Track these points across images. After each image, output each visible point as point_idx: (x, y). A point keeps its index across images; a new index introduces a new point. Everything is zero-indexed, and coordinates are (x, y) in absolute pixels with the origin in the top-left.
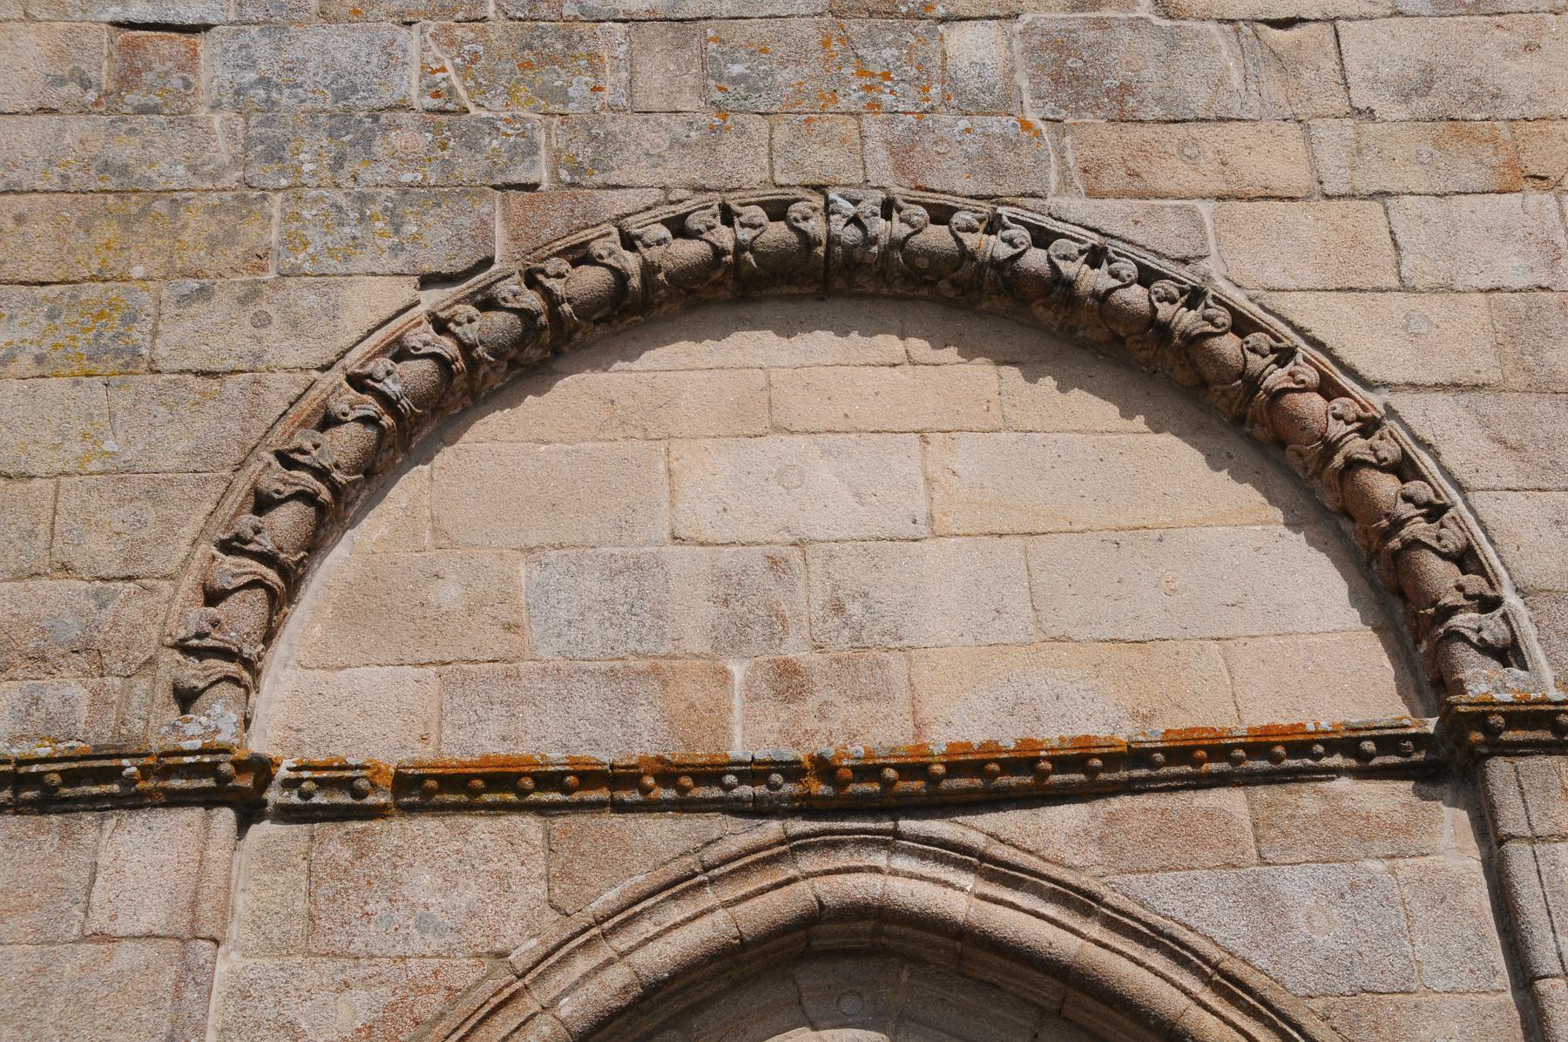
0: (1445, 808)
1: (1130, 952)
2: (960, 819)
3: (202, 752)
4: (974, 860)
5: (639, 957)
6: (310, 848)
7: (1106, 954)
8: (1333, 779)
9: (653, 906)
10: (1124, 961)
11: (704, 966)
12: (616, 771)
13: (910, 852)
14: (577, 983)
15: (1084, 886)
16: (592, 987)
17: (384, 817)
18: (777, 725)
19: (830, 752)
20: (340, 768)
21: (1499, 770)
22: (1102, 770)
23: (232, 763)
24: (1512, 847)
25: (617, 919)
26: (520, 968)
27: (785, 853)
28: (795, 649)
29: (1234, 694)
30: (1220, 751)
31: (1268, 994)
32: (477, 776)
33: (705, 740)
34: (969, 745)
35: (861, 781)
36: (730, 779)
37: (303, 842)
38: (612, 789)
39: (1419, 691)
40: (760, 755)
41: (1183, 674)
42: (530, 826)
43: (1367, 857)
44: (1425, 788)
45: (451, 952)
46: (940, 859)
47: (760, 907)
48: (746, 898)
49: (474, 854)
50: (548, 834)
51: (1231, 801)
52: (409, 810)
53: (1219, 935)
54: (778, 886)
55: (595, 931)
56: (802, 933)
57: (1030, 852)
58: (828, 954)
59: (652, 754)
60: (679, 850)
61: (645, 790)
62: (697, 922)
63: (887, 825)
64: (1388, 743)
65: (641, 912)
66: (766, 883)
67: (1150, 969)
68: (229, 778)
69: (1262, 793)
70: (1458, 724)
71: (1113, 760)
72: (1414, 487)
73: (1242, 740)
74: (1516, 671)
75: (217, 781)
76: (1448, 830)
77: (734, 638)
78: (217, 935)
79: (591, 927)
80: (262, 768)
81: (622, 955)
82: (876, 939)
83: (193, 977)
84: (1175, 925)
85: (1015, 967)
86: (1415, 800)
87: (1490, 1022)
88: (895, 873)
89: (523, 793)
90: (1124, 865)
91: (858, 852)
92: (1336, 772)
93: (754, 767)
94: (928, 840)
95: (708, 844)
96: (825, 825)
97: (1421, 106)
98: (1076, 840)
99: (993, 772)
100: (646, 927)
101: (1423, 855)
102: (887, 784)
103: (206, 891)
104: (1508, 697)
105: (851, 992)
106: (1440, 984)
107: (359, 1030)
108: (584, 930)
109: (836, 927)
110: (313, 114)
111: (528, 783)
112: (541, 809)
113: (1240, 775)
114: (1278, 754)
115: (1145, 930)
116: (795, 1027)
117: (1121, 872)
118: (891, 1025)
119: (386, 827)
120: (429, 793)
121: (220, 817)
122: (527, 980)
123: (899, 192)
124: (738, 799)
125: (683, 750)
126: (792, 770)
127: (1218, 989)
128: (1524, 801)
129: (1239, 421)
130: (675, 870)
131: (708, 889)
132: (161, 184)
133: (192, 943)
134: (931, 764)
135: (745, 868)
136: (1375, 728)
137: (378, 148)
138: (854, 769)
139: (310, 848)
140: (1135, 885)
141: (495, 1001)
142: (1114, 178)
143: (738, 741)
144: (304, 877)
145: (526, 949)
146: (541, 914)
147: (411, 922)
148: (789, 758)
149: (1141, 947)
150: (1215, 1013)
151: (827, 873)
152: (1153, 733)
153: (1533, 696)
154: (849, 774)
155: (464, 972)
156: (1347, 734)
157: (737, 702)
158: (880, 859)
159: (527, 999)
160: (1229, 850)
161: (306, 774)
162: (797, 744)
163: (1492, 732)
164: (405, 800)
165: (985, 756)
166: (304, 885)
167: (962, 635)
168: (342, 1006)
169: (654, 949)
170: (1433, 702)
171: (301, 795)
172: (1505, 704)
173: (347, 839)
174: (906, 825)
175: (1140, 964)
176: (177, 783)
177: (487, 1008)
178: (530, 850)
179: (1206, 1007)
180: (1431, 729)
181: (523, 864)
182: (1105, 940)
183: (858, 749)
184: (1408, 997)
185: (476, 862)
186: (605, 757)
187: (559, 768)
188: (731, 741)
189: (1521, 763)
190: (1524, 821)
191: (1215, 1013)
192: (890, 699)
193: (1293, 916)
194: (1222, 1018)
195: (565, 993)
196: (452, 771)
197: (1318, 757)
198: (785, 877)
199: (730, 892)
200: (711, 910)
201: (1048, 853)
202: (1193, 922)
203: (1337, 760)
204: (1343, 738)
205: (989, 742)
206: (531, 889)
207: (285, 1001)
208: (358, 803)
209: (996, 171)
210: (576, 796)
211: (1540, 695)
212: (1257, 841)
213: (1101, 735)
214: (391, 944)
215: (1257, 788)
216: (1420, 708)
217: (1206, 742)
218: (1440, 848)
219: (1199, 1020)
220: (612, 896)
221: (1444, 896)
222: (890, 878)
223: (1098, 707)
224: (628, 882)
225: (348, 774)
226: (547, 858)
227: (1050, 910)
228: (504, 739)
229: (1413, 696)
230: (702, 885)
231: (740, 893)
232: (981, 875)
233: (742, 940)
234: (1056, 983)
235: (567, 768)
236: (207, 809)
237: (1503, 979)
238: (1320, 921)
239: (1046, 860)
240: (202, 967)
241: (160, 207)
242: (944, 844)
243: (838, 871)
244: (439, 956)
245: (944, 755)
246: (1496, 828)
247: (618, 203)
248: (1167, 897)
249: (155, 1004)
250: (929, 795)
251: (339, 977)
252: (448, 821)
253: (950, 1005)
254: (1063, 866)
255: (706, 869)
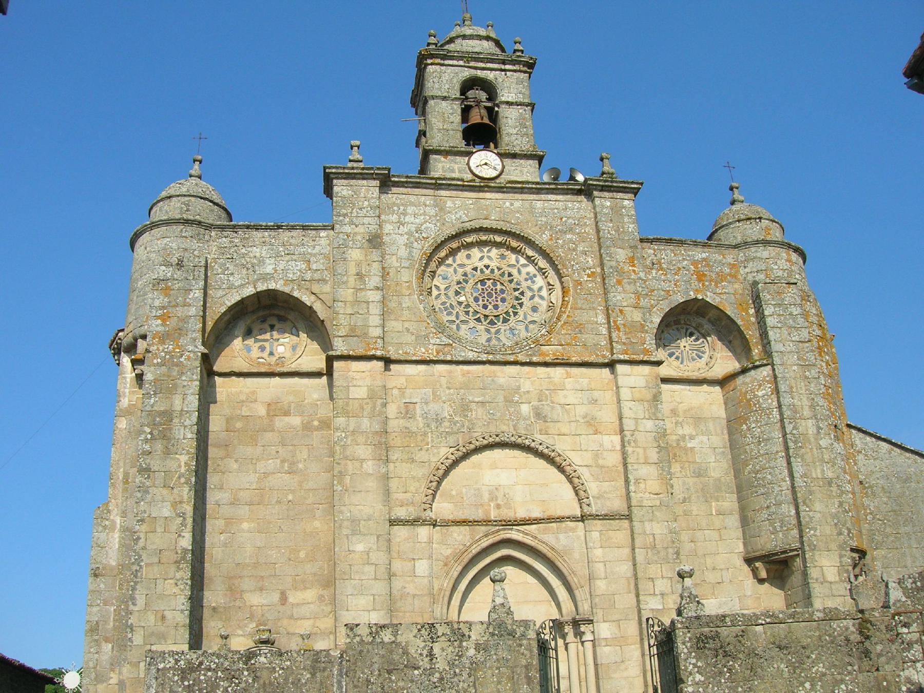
28: (499, 502)
42: (467, 527)
69: (558, 524)
72: (580, 481)
77: (491, 500)
97: (585, 420)
110: (433, 419)
123: (514, 433)
129: (559, 467)
132: (413, 431)
137: (442, 425)
142: (543, 432)
145: (468, 544)
155: (461, 547)
157: (492, 509)
158: (510, 532)
209: (528, 430)
241: (414, 434)
247: (475, 435)
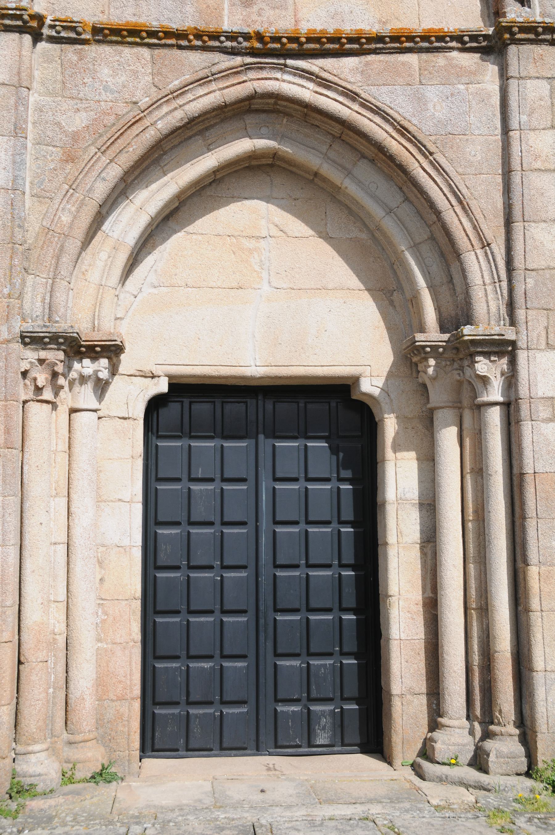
0: (490, 65)
1: (368, 116)
2: (310, 61)
3: (16, 9)
4: (314, 77)
5: (187, 107)
6: (61, 55)
7: (359, 116)
8: (451, 52)
9: (192, 88)
10: (366, 119)
11: (211, 113)
12: (179, 32)
13: (290, 73)
14: (164, 116)
15: (354, 90)
16: (169, 118)
17: (89, 44)
18: (241, 17)
19: (261, 30)
20: (71, 22)
21: (513, 49)
22: (366, 44)
23: (28, 15)
24: (511, 81)
25: (179, 92)
26: (143, 109)
27: (243, 70)
29: (419, 15)
30: (410, 38)
31: (416, 134)
32: (124, 30)
33: (213, 22)
34: (315, 30)
35: (273, 42)
36: (223, 39)
37: (58, 52)
38: (177, 40)
39: (489, 16)
40: (235, 30)
41: (400, 5)
42: (145, 52)
43: (459, 83)
44: (485, 57)
45: (116, 101)
46: (301, 76)
47: (233, 91)
48: (227, 87)
49: (124, 62)
50: (152, 56)
51: (412, 59)
52: (98, 42)
53: (401, 111)
54: (239, 83)
55: (170, 96)
56: (247, 103)
57: (335, 76)
58: (257, 111)
59: (193, 26)
60: (202, 66)
61: (190, 41)
62: (209, 95)
63: (282, 61)
64: (474, 38)
65: (188, 90)
66: (235, 82)
67: (374, 123)
68: (28, 22)
69: (424, 56)
70: (500, 30)
71: (370, 40)
73: (420, 34)
74: (526, 8)
75: (23, 23)
76: (489, 73)
78: (29, 86)
79: (169, 94)
80: (40, 18)
81: (181, 106)
82: (275, 106)
83: (21, 102)
84: (386, 107)
85: (326, 120)
86: (480, 61)
87: (491, 146)
88: (284, 81)
89: (142, 38)
90: (370, 82)
91: (270, 71)
92: (452, 49)
93: (232, 34)
94: (297, 69)
95: (214, 64)
96: (258, 60)
98: (353, 72)
99: (324, 42)
100: (190, 96)
101: (479, 83)
102: (283, 44)
103: (23, 68)
104: (521, 20)
105: (265, 126)
106: (477, 132)
107: (84, 127)
108: (166, 96)
109: (260, 101)
111: (144, 34)
112: (150, 46)
113: (417, 48)
114: (432, 41)
115: (375, 108)
116: (244, 138)
117: (368, 85)
118: (279, 139)
119: (90, 49)
120: (105, 36)
121: (25, 38)
122: (145, 113)
124: (225, 47)
125: (205, 25)
126: (247, 37)
127: (398, 131)
128: (519, 63)
130: (201, 74)
131: (213, 83)
133: (20, 88)
134: (300, 37)
135: (227, 75)
136: (470, 31)
138: (271, 37)
139: (61, 55)
140: (373, 90)
141: (134, 120)
143: (226, 23)
144: (59, 66)
145: (145, 102)
146: (150, 88)
147: (101, 87)
148: (246, 31)
149: (373, 114)
150: (396, 140)
151: (258, 79)
152: (386, 30)
153: (531, 19)
154: (268, 39)
155: (122, 109)
156: (459, 33)
158: (278, 75)
159: (145, 121)
160: (409, 79)
161: (57, 23)
162: (249, 26)
163: (512, 34)
164: (97, 38)
165: (321, 35)
166: (60, 69)
167: (37, 466)
168: (77, 118)
169: (193, 104)
170: (493, 21)
171: (56, 32)
172: (520, 22)
173: (76, 52)
174: (290, 62)
175: (371, 121)
176: (7, 22)
177: (131, 123)
178: (146, 62)
179: (393, 138)
180: (490, 33)
181: (143, 68)
182: (360, 111)
183: (273, 29)
184: (465, 136)
185: (125, 66)
186: (175, 25)
187: (156, 29)
188: (223, 22)
189: (521, 47)
190: (517, 71)
191: (396, 140)
192: (286, 9)
193: (429, 105)
194: (398, 142)
195: (159, 119)
196: (114, 27)
197: (446, 42)
198: (242, 80)
199: (221, 84)
200: (214, 91)
201: (342, 76)
202: (392, 106)
203: (454, 44)
204: (458, 35)
205: (324, 29)
206: (146, 78)
207: (56, 114)
208: (79, 37)
210: (163, 42)
211: (533, 19)
212: (420, 75)
213: (366, 29)
214: (94, 95)
215: (423, 54)
216: (488, 23)
217: (406, 34)
218: (486, 81)
219: (390, 142)
220: (177, 83)
221: (483, 99)
222: (282, 83)
223: (366, 17)
224: (183, 78)
225: (74, 25)
226: (152, 66)
227: (341, 99)
228: (134, 15)
229: (486, 18)
230: (211, 81)
231: (225, 85)
232: (316, 83)
233: (225, 103)
234: (340, 127)
235: (160, 29)
236: (20, 34)
237: (499, 131)
238: (438, 107)
239: (341, 79)
240: (24, 98)
242: (303, 71)
243: (262, 79)
244: (112, 101)
245: (306, 34)
246: (507, 74)
248: (384, 96)
249: (8, 111)
250: (299, 50)
251: (75, 107)
252: (114, 48)
253: (301, 133)
254: (347, 81)
255: (213, 75)
